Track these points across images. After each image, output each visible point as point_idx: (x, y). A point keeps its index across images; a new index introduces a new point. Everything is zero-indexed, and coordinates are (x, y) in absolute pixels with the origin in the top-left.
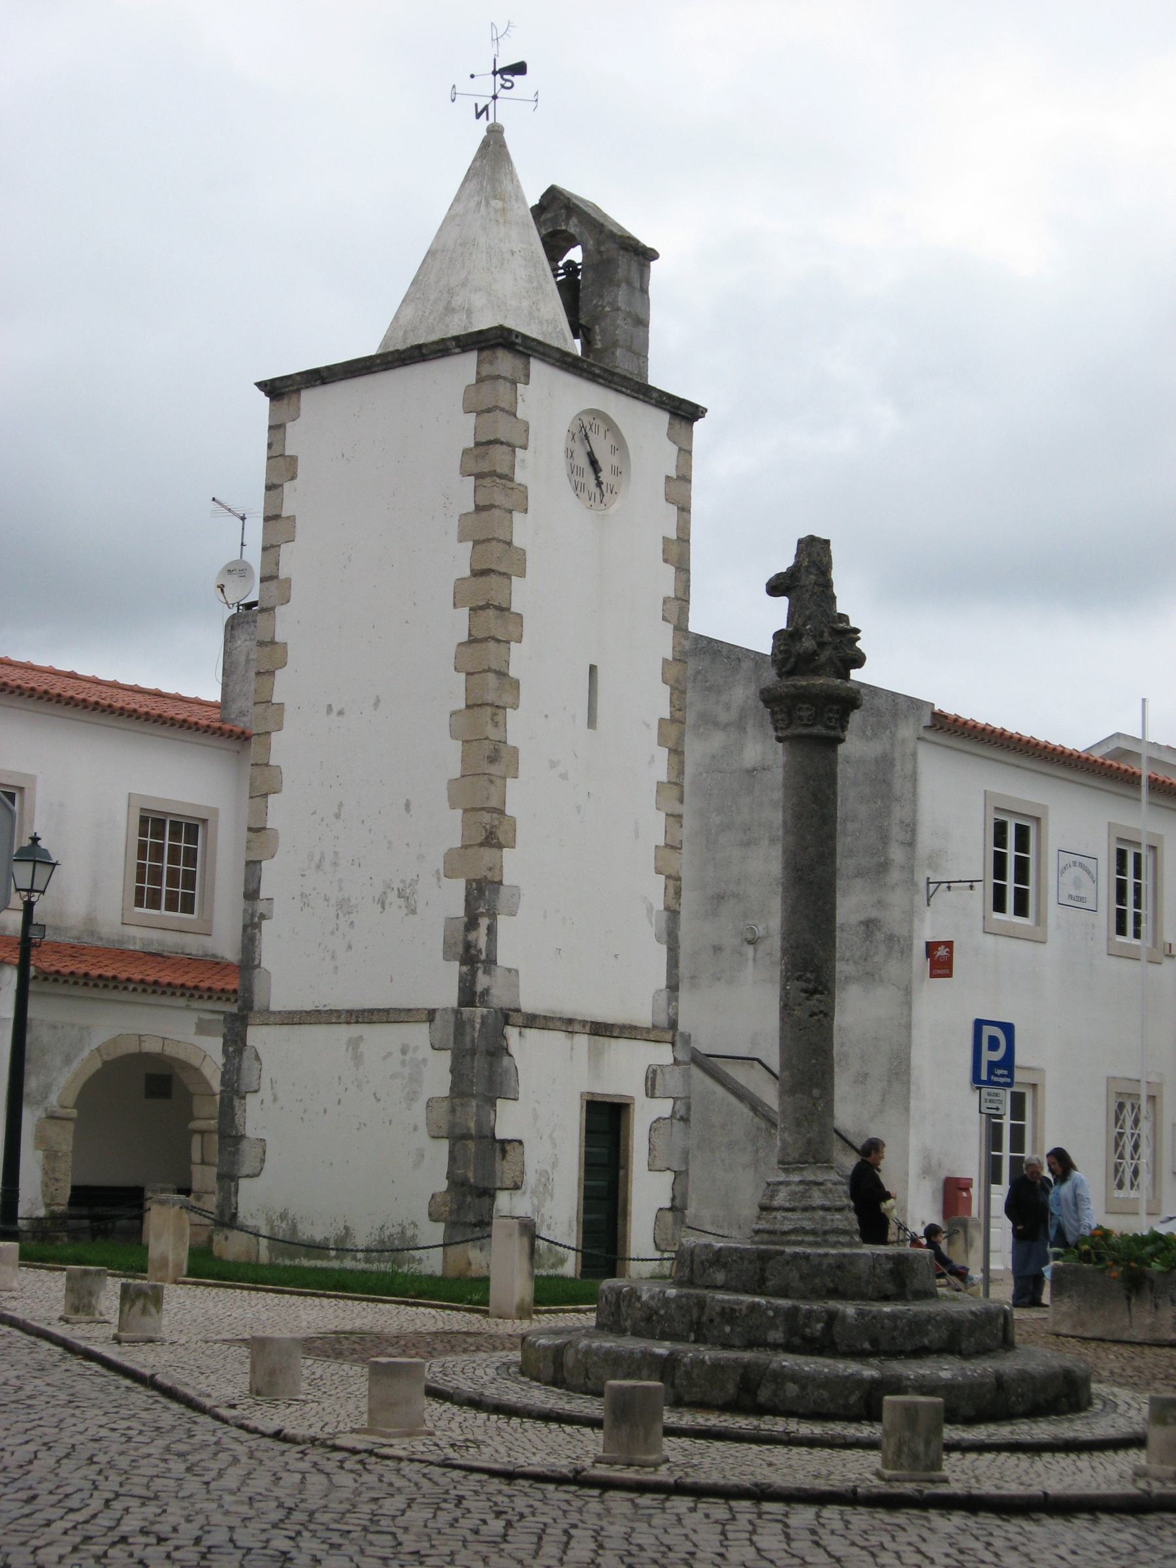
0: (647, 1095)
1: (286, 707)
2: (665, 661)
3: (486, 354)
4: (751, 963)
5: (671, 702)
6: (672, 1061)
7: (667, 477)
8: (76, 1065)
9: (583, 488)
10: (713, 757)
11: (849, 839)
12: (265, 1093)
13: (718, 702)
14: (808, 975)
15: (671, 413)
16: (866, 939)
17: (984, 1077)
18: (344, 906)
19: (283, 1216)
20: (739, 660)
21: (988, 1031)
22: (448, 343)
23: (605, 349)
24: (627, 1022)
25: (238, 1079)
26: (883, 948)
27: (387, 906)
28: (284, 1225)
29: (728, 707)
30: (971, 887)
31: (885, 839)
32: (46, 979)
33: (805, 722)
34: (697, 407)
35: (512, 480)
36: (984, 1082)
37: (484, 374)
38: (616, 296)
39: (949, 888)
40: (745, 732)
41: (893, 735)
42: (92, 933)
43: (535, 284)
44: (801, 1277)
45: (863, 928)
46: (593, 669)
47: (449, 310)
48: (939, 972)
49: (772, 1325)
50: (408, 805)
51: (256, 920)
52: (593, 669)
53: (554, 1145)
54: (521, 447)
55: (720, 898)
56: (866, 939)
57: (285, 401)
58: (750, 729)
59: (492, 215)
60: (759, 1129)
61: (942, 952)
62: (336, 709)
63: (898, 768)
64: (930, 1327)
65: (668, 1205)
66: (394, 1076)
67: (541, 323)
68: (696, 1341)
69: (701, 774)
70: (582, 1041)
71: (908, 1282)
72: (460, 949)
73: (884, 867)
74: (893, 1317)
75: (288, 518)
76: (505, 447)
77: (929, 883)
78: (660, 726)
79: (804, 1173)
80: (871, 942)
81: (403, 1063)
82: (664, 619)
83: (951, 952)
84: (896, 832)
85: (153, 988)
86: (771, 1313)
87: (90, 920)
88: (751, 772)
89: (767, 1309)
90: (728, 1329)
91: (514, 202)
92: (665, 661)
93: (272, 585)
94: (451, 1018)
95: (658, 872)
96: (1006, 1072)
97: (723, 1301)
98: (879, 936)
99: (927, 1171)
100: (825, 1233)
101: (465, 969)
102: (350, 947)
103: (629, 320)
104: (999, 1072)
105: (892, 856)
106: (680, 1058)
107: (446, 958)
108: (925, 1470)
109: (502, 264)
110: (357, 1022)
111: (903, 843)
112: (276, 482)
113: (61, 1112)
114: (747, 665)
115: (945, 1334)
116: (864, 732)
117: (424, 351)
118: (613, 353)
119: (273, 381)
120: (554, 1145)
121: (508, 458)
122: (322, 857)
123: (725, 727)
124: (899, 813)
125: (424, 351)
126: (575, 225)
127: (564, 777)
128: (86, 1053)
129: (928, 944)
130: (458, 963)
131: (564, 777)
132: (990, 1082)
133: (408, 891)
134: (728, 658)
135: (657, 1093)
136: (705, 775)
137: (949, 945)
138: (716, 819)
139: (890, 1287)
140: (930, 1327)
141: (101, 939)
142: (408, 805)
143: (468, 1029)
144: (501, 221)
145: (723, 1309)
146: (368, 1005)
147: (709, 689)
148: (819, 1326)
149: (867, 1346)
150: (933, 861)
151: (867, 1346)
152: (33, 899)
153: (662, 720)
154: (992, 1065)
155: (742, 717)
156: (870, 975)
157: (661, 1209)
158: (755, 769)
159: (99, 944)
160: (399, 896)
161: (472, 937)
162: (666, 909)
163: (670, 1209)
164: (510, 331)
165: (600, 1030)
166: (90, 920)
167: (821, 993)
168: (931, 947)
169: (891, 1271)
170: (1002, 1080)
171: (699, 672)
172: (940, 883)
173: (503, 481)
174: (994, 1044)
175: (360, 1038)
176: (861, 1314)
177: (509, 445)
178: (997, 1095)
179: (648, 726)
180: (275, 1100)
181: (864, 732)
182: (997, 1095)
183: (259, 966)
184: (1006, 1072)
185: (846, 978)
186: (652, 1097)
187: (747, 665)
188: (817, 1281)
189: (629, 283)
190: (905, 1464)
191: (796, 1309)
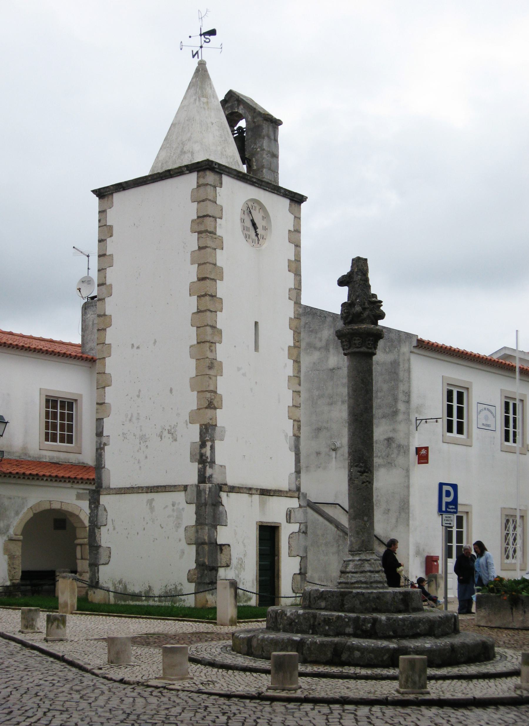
0: (287, 522)
2: (290, 319)
4: (334, 459)
5: (294, 338)
6: (298, 506)
7: (289, 231)
8: (21, 515)
10: (314, 363)
12: (110, 526)
13: (316, 338)
15: (290, 199)
16: (388, 447)
17: (444, 509)
18: (143, 438)
19: (120, 582)
20: (325, 317)
21: (445, 488)
23: (258, 169)
27: (163, 438)
28: (121, 586)
29: (321, 340)
30: (437, 421)
34: (303, 196)
35: (215, 234)
36: (444, 512)
37: (200, 183)
38: (263, 144)
41: (399, 351)
42: (26, 454)
43: (223, 139)
45: (386, 442)
46: (256, 323)
48: (422, 461)
51: (102, 446)
52: (256, 323)
53: (245, 546)
54: (219, 218)
56: (388, 447)
57: (106, 199)
59: (202, 105)
60: (339, 536)
61: (423, 452)
62: (136, 346)
63: (401, 366)
64: (420, 624)
65: (298, 572)
67: (227, 157)
68: (312, 634)
69: (308, 371)
70: (256, 498)
71: (410, 604)
73: (395, 413)
74: (403, 620)
75: (110, 255)
76: (211, 218)
77: (417, 420)
78: (289, 350)
80: (390, 448)
81: (173, 510)
83: (427, 452)
85: (55, 479)
86: (347, 620)
87: (25, 448)
88: (332, 370)
89: (345, 618)
90: (327, 628)
92: (290, 319)
95: (290, 418)
96: (454, 507)
97: (325, 615)
98: (394, 445)
99: (418, 553)
100: (371, 583)
101: (200, 466)
103: (269, 155)
104: (451, 507)
105: (399, 408)
106: (302, 504)
107: (191, 461)
109: (207, 129)
110: (151, 492)
112: (103, 238)
113: (15, 537)
114: (329, 319)
118: (262, 171)
120: (245, 546)
121: (213, 223)
122: (132, 416)
126: (242, 109)
127: (244, 375)
128: (25, 510)
130: (197, 463)
131: (244, 375)
132: (446, 512)
133: (173, 430)
134: (320, 316)
135: (292, 521)
136: (310, 372)
137: (427, 448)
138: (316, 393)
139: (402, 607)
140: (420, 624)
141: (30, 457)
143: (203, 494)
144: (206, 108)
147: (312, 331)
148: (369, 625)
149: (391, 633)
150: (418, 410)
151: (391, 633)
153: (289, 347)
154: (447, 504)
156: (390, 463)
157: (295, 574)
158: (334, 369)
159: (29, 459)
160: (169, 433)
161: (203, 451)
164: (212, 162)
165: (264, 492)
166: (25, 448)
167: (367, 472)
168: (418, 450)
169: (402, 599)
170: (452, 510)
173: (211, 235)
175: (153, 499)
176: (388, 619)
177: (213, 217)
178: (450, 517)
180: (114, 529)
181: (385, 350)
182: (450, 517)
183: (104, 467)
184: (454, 507)
185: (379, 465)
186: (290, 523)
187: (329, 319)
189: (269, 137)
191: (358, 618)
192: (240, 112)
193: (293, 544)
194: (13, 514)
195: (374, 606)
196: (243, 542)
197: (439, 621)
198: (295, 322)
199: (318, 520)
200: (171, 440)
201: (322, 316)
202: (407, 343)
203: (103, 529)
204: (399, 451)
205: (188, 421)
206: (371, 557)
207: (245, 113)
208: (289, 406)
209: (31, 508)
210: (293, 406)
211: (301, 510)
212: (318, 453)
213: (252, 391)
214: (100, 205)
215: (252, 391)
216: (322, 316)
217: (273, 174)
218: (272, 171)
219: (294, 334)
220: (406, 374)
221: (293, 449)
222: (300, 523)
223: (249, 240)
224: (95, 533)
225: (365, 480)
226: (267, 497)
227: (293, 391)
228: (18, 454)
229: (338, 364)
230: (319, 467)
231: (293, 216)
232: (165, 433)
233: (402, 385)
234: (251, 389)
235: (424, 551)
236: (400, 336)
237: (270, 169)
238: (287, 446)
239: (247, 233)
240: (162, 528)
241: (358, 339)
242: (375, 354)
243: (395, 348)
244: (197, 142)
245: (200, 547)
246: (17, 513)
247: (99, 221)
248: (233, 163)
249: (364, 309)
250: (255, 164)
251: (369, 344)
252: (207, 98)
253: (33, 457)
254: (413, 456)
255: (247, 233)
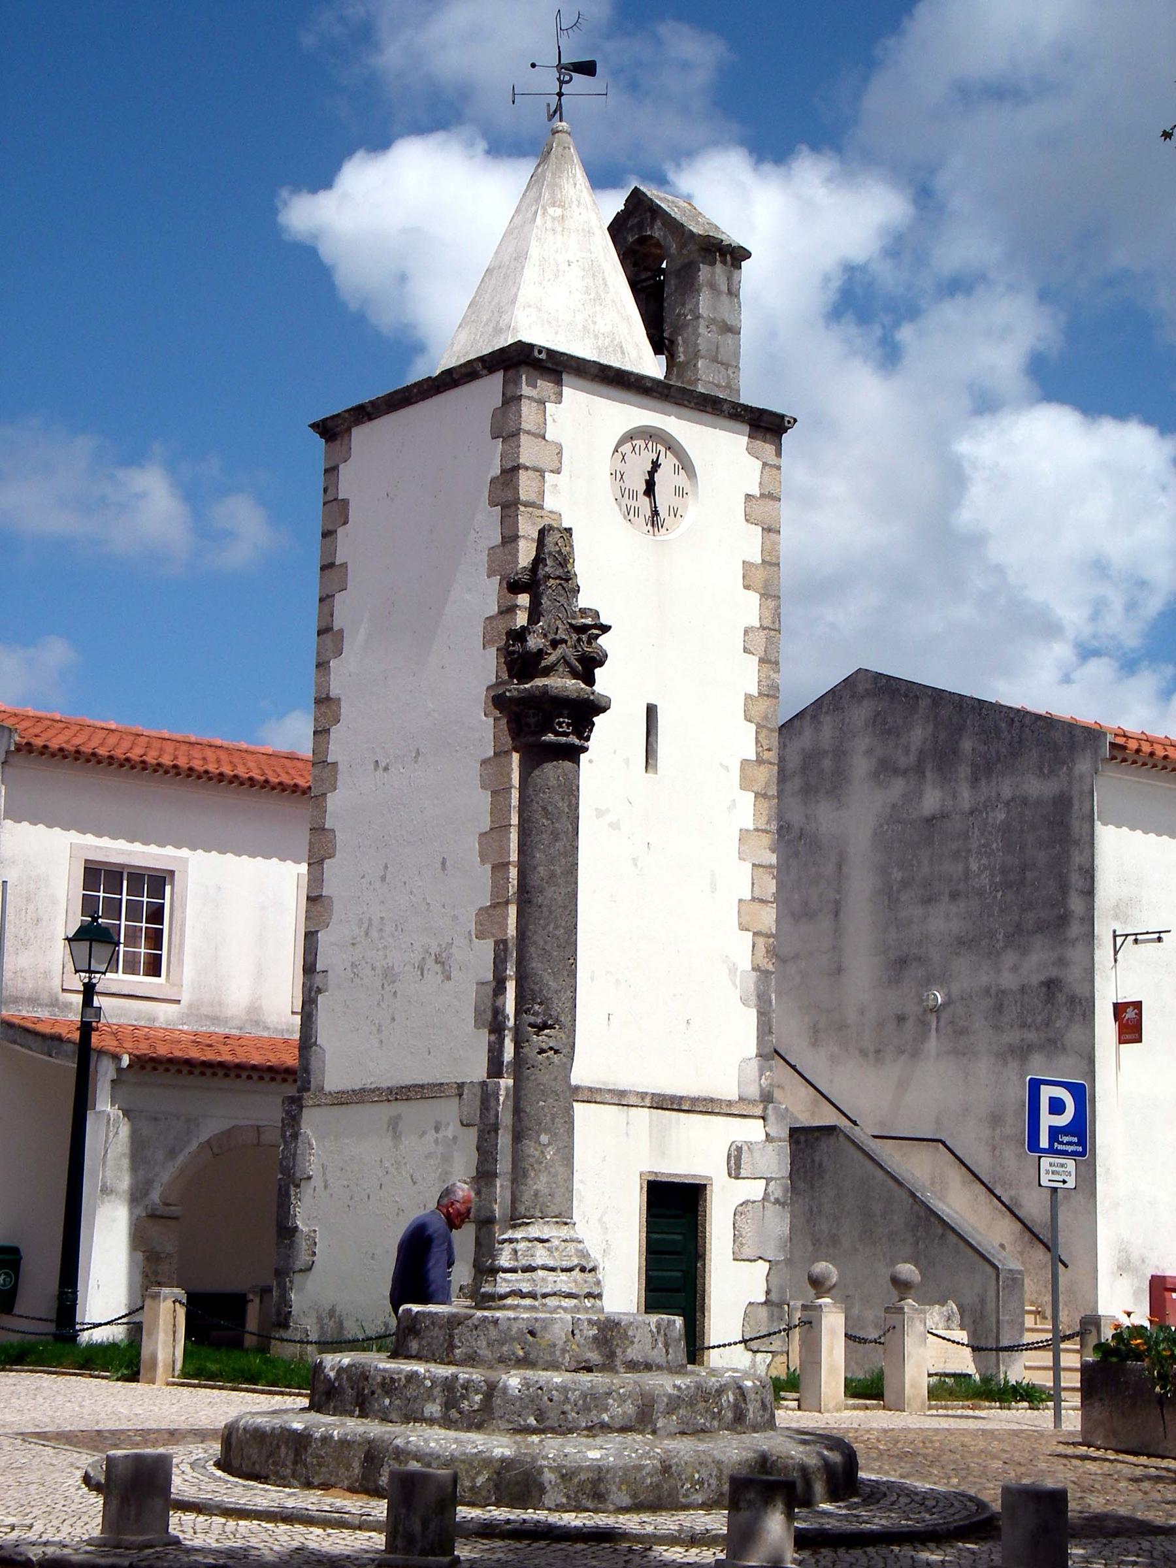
0: (730, 1175)
1: (340, 767)
2: (748, 697)
3: (511, 373)
4: (933, 1033)
5: (757, 741)
6: (763, 1137)
7: (748, 496)
8: (181, 1159)
9: (637, 513)
10: (894, 806)
11: (1028, 891)
12: (317, 1181)
13: (897, 745)
14: (537, 1007)
15: (750, 425)
16: (1047, 1002)
17: (1044, 1143)
18: (389, 975)
19: (332, 1312)
20: (917, 697)
21: (1046, 1092)
22: (475, 365)
23: (687, 363)
24: (704, 1094)
25: (294, 1166)
26: (1064, 1011)
27: (425, 972)
28: (331, 1323)
29: (907, 751)
30: (1159, 939)
31: (1064, 889)
32: (143, 1068)
33: (533, 728)
34: (782, 417)
35: (542, 508)
36: (1044, 1151)
37: (509, 394)
38: (698, 303)
39: (1136, 941)
40: (924, 776)
41: (1070, 770)
42: (257, 1023)
43: (592, 296)
44: (488, 1344)
45: (1044, 989)
46: (651, 711)
47: (498, 331)
48: (1128, 1037)
49: (430, 1397)
50: (444, 863)
51: (313, 994)
52: (651, 711)
53: (606, 1230)
54: (552, 471)
55: (902, 963)
56: (1047, 1002)
57: (338, 442)
58: (928, 774)
59: (549, 225)
60: (918, 1217)
61: (1130, 1014)
62: (382, 765)
63: (1076, 807)
64: (611, 1401)
65: (763, 1299)
66: (429, 1156)
67: (597, 337)
68: (359, 1417)
69: (881, 826)
70: (643, 1116)
71: (619, 1351)
72: (489, 1016)
73: (1063, 920)
74: (564, 1389)
75: (341, 565)
76: (530, 472)
77: (1115, 937)
78: (742, 769)
79: (530, 1228)
80: (1053, 1004)
81: (436, 1142)
82: (746, 650)
83: (1140, 1014)
84: (1076, 880)
85: (283, 1075)
86: (428, 1383)
87: (254, 1010)
88: (930, 821)
89: (425, 1378)
90: (387, 1401)
91: (574, 207)
92: (748, 697)
93: (327, 637)
94: (477, 1090)
95: (743, 928)
96: (1075, 1140)
97: (385, 1370)
98: (1061, 998)
99: (1124, 1267)
100: (545, 1296)
101: (493, 1037)
102: (393, 1019)
103: (713, 327)
104: (1066, 1139)
105: (1073, 907)
106: (773, 1133)
107: (477, 1026)
108: (420, 1555)
109: (556, 277)
110: (396, 1099)
111: (1082, 892)
112: (331, 528)
113: (162, 1210)
114: (924, 703)
115: (630, 1408)
116: (1041, 770)
117: (455, 376)
118: (695, 365)
119: (324, 421)
120: (606, 1230)
121: (535, 484)
122: (370, 925)
123: (904, 773)
124: (1077, 859)
125: (455, 376)
126: (659, 229)
127: (615, 826)
128: (194, 1146)
129: (1116, 1006)
130: (486, 1031)
131: (615, 826)
132: (1052, 1151)
133: (444, 955)
134: (906, 696)
135: (743, 1173)
136: (886, 827)
137: (1138, 1005)
138: (897, 875)
139: (594, 1357)
140: (611, 1401)
141: (267, 1028)
142: (444, 863)
143: (493, 1103)
144: (559, 229)
145: (384, 1378)
146: (408, 1081)
147: (889, 732)
148: (478, 1398)
149: (532, 1421)
150: (1119, 912)
151: (532, 1421)
152: (94, 981)
153: (745, 762)
154: (1054, 1132)
155: (921, 761)
156: (1052, 1042)
157: (750, 1304)
158: (934, 817)
159: (265, 1034)
160: (437, 962)
161: (499, 1003)
162: (753, 969)
163: (765, 1303)
164: (531, 346)
165: (665, 1103)
166: (254, 1010)
167: (551, 1027)
168: (1119, 1009)
169: (595, 1338)
170: (1070, 1148)
171: (879, 714)
172: (1127, 935)
173: (530, 509)
174: (1057, 1107)
175: (399, 1117)
176: (526, 1384)
177: (536, 470)
178: (1062, 1165)
179: (727, 768)
180: (326, 1187)
181: (1041, 770)
182: (1062, 1165)
183: (315, 1044)
184: (1075, 1140)
185: (1028, 1046)
186: (737, 1178)
187: (924, 703)
188: (505, 1348)
189: (713, 287)
190: (400, 1545)
191: (455, 1377)
192: (656, 235)
193: (748, 1229)
194: (160, 1156)
195: (521, 1353)
196: (600, 1220)
197: (670, 1396)
198: (763, 705)
199: (874, 1178)
200: (440, 977)
201: (911, 695)
202: (1089, 753)
203: (307, 1190)
204: (1074, 1011)
205: (473, 933)
206: (554, 1234)
207: (665, 237)
208: (740, 900)
209: (208, 1142)
210: (753, 899)
211: (770, 1147)
212: (901, 1019)
213: (636, 865)
214: (328, 455)
215: (636, 865)
216: (911, 695)
217: (722, 369)
218: (722, 364)
219: (757, 733)
220: (1087, 826)
221: (753, 999)
222: (768, 1180)
223: (635, 519)
224: (288, 1195)
225: (544, 1046)
226: (674, 1114)
227: (754, 865)
228: (237, 1023)
229: (943, 805)
230: (903, 1052)
231: (758, 464)
232: (430, 961)
233: (1077, 853)
234: (635, 861)
235: (1143, 1261)
236: (1072, 736)
237: (715, 360)
238: (737, 993)
239: (633, 503)
240: (415, 1183)
241: (534, 715)
242: (586, 749)
243: (1063, 763)
244: (529, 306)
245: (484, 1229)
246: (172, 1154)
247: (325, 490)
248: (610, 349)
249: (555, 644)
250: (681, 349)
251: (560, 724)
252: (563, 207)
253: (276, 1030)
254: (1105, 1026)
255: (633, 503)
